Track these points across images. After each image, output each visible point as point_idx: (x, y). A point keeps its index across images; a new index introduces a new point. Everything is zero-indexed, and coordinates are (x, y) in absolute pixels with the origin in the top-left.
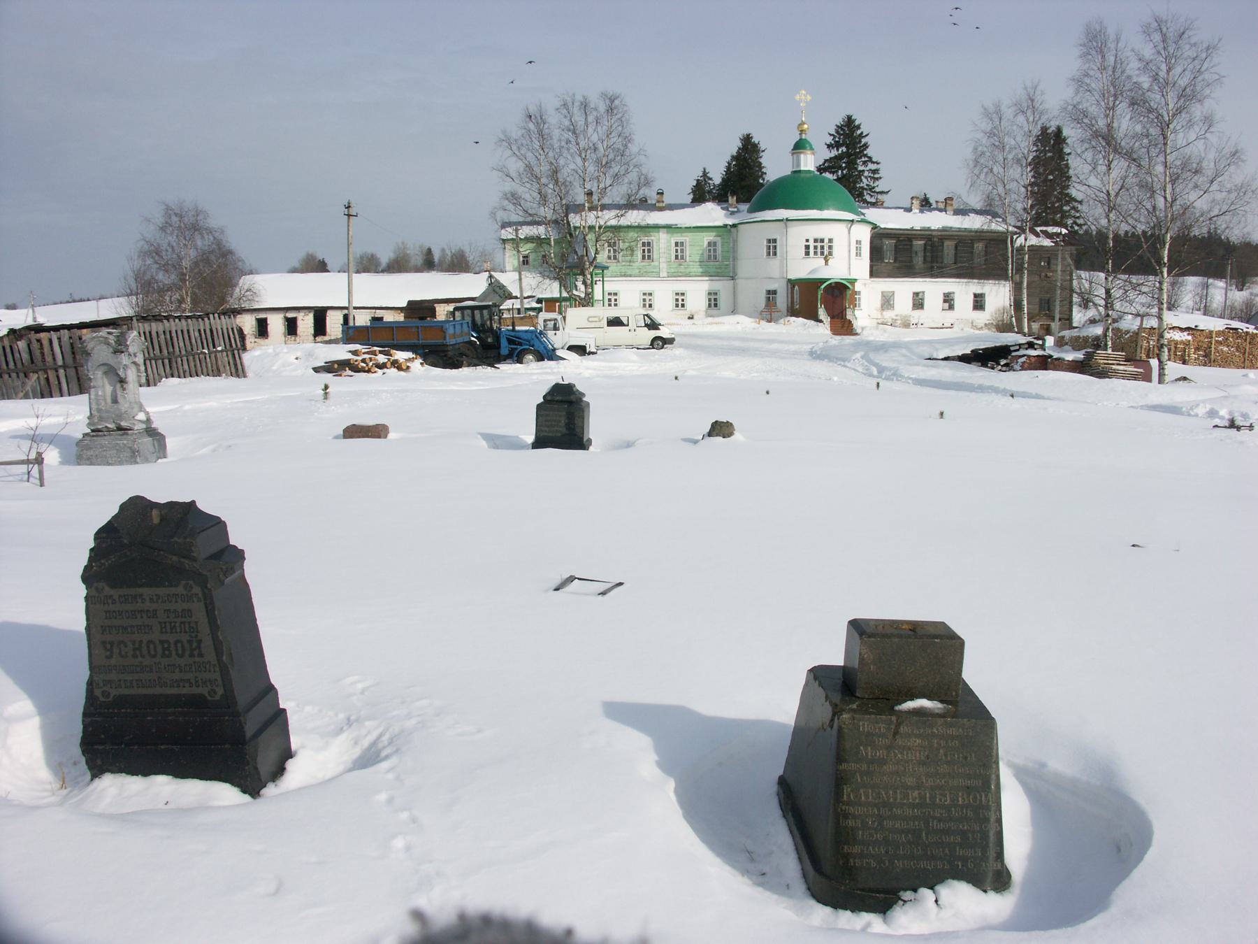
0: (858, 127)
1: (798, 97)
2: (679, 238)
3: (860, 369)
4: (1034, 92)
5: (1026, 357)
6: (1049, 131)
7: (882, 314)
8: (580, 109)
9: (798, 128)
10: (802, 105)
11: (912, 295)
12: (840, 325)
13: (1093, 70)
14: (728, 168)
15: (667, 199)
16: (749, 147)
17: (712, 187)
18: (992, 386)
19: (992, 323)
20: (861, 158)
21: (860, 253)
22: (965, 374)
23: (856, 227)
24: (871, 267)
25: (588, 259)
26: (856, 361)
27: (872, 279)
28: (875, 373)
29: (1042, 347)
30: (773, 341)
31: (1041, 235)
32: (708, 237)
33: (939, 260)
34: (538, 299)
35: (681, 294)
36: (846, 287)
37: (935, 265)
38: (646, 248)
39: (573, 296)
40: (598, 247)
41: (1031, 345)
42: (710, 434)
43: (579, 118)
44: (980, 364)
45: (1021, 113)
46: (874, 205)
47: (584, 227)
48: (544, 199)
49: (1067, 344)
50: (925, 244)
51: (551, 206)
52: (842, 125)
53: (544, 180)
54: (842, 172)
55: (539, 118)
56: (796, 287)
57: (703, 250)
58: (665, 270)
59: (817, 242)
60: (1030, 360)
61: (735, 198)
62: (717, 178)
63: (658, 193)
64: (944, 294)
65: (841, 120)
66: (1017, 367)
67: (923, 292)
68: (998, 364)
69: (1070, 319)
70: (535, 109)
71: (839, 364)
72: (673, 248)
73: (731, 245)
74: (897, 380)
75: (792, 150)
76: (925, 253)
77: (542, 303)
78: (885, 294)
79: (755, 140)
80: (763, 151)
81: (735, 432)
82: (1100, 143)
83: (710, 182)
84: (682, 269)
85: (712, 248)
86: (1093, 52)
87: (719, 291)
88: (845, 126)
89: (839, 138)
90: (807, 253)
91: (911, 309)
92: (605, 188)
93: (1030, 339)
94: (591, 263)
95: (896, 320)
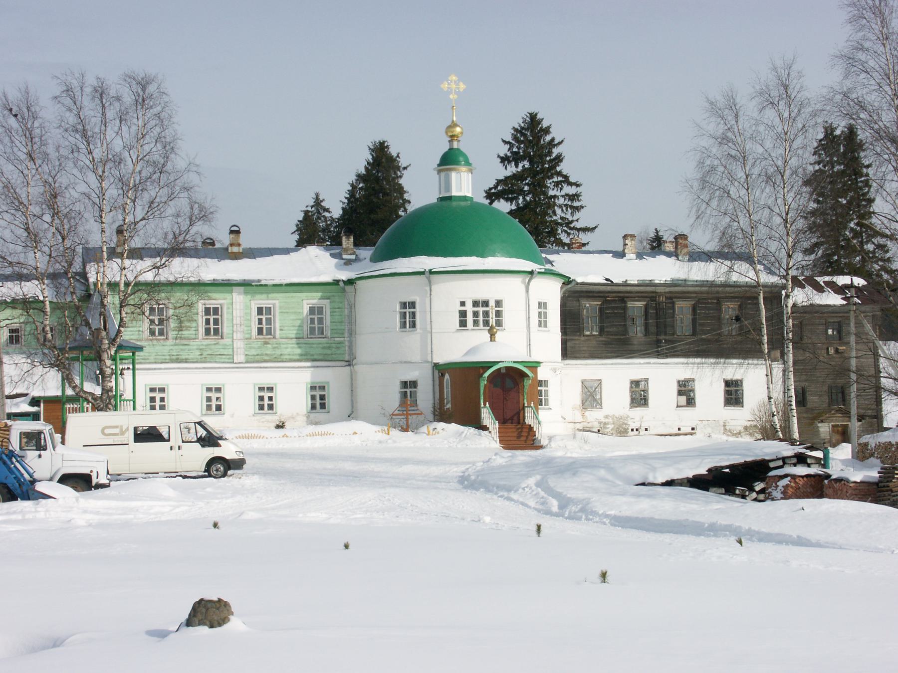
0: (547, 131)
1: (445, 86)
2: (263, 301)
3: (532, 503)
4: (789, 75)
5: (789, 478)
6: (838, 132)
7: (583, 415)
8: (93, 98)
9: (446, 133)
10: (451, 97)
11: (628, 385)
12: (515, 434)
13: (870, 40)
14: (352, 193)
15: (246, 241)
16: (383, 160)
17: (329, 223)
18: (730, 526)
19: (756, 426)
20: (551, 177)
21: (545, 322)
22: (695, 507)
23: (538, 283)
24: (564, 343)
25: (108, 333)
26: (527, 489)
27: (568, 362)
28: (555, 509)
29: (824, 462)
30: (405, 461)
31: (826, 288)
32: (312, 299)
33: (669, 330)
34: (33, 398)
35: (268, 388)
36: (523, 375)
37: (662, 337)
38: (212, 318)
39: (82, 394)
40: (124, 315)
41: (801, 459)
42: (189, 623)
43: (91, 109)
44: (723, 490)
45: (770, 106)
46: (570, 247)
47: (102, 284)
48: (33, 238)
49: (872, 455)
50: (646, 307)
51: (46, 249)
52: (522, 128)
53: (35, 209)
54: (524, 198)
55: (25, 110)
56: (447, 376)
57: (302, 320)
58: (241, 351)
59: (478, 306)
60: (796, 482)
61: (352, 239)
62: (335, 208)
63: (232, 232)
64: (679, 382)
65: (521, 121)
66: (777, 494)
67: (646, 380)
68: (752, 489)
69: (878, 417)
70: (19, 95)
71: (501, 496)
72: (255, 317)
73: (346, 312)
74: (587, 519)
75: (439, 165)
76: (646, 319)
77: (39, 406)
78: (587, 384)
79: (393, 151)
80: (405, 168)
81: (231, 617)
82: (888, 149)
83: (327, 214)
84: (268, 349)
85: (316, 317)
86: (868, 15)
87: (328, 383)
88: (526, 129)
89: (519, 148)
90: (463, 324)
91: (628, 406)
92: (136, 223)
93: (800, 449)
94: (112, 341)
95: (605, 424)
